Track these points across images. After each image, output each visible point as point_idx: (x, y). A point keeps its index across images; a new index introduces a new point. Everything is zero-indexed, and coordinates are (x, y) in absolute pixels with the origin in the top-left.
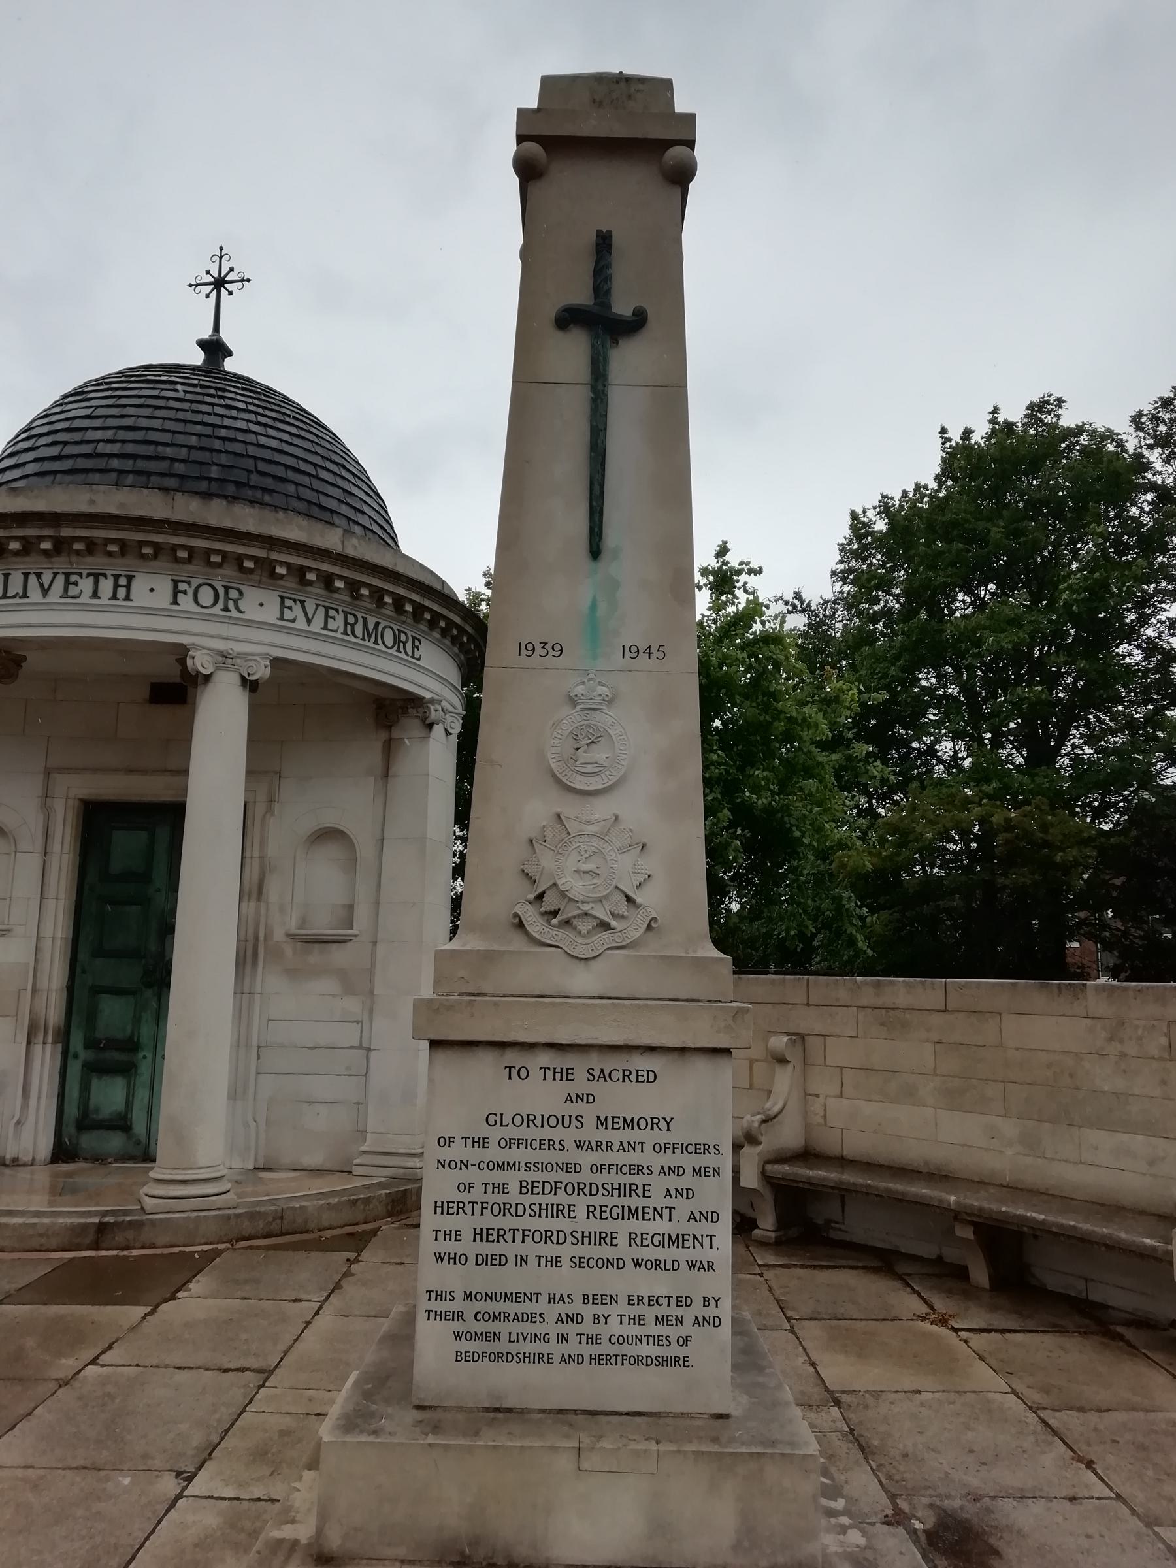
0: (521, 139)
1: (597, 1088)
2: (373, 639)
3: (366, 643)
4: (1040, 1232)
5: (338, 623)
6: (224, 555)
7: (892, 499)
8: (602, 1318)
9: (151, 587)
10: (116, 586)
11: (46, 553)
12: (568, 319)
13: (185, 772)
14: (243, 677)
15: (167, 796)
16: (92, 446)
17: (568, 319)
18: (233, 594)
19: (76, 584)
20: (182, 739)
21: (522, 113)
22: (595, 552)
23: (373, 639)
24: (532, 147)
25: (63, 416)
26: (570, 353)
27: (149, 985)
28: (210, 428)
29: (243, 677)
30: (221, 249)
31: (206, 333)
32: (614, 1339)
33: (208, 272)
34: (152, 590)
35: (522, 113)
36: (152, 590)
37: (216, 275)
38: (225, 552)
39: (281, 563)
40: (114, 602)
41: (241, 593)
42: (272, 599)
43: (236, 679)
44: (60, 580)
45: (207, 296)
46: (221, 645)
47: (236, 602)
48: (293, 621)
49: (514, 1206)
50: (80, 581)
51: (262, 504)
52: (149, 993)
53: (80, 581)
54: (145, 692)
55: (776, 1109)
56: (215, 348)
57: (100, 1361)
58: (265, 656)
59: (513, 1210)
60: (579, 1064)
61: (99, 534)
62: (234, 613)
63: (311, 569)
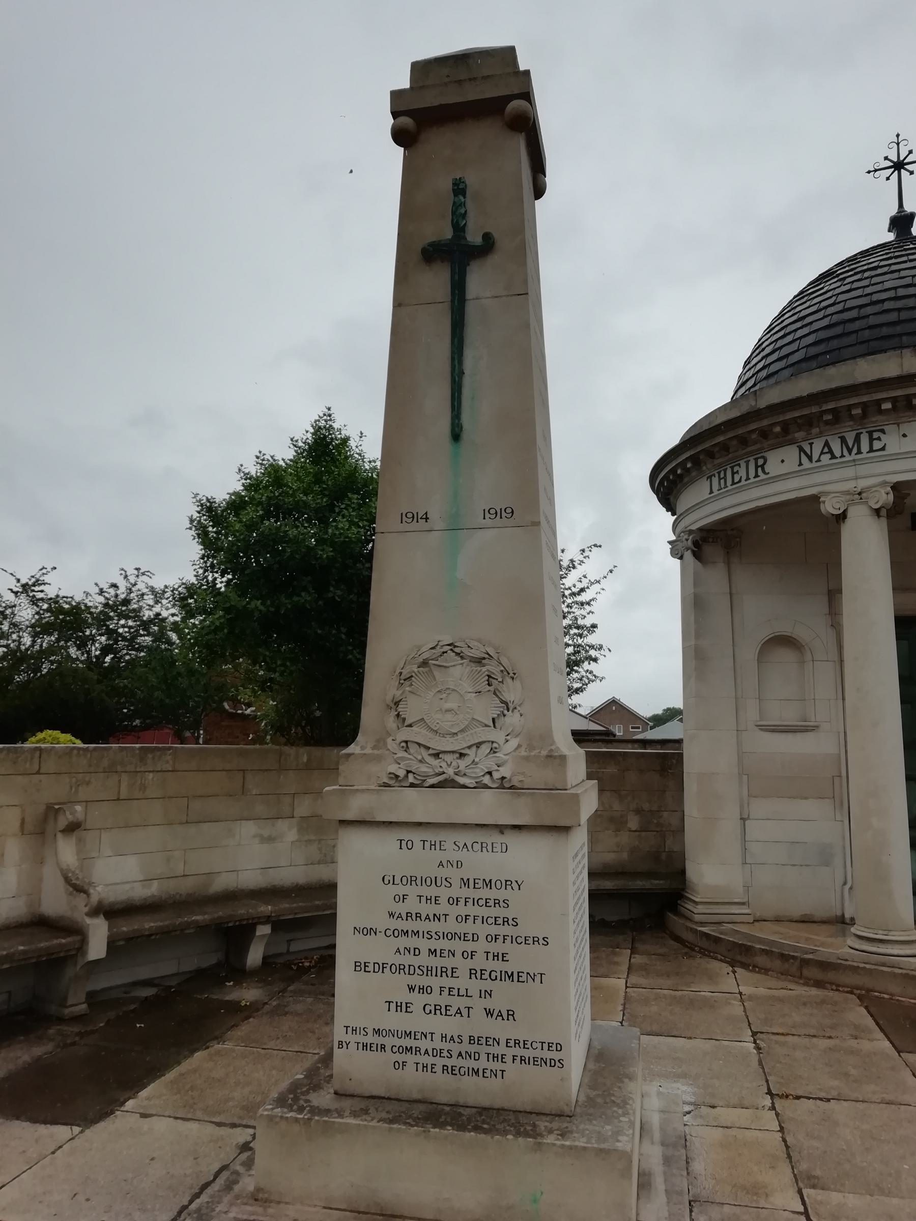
0: (395, 114)
1: (462, 855)
2: (855, 450)
8: (344, 1044)
9: (782, 461)
10: (720, 479)
12: (432, 253)
16: (854, 336)
17: (432, 253)
18: (760, 462)
21: (396, 96)
22: (456, 436)
23: (855, 450)
24: (406, 120)
25: (799, 324)
26: (436, 281)
28: (893, 291)
30: (898, 136)
31: (894, 211)
32: (395, 1049)
33: (886, 158)
34: (783, 461)
35: (396, 96)
36: (783, 461)
37: (895, 160)
38: (864, 403)
39: (885, 400)
41: (763, 457)
42: (790, 454)
45: (888, 179)
46: (849, 486)
47: (762, 467)
48: (883, 449)
49: (407, 967)
56: (901, 222)
59: (407, 970)
60: (449, 838)
62: (762, 476)
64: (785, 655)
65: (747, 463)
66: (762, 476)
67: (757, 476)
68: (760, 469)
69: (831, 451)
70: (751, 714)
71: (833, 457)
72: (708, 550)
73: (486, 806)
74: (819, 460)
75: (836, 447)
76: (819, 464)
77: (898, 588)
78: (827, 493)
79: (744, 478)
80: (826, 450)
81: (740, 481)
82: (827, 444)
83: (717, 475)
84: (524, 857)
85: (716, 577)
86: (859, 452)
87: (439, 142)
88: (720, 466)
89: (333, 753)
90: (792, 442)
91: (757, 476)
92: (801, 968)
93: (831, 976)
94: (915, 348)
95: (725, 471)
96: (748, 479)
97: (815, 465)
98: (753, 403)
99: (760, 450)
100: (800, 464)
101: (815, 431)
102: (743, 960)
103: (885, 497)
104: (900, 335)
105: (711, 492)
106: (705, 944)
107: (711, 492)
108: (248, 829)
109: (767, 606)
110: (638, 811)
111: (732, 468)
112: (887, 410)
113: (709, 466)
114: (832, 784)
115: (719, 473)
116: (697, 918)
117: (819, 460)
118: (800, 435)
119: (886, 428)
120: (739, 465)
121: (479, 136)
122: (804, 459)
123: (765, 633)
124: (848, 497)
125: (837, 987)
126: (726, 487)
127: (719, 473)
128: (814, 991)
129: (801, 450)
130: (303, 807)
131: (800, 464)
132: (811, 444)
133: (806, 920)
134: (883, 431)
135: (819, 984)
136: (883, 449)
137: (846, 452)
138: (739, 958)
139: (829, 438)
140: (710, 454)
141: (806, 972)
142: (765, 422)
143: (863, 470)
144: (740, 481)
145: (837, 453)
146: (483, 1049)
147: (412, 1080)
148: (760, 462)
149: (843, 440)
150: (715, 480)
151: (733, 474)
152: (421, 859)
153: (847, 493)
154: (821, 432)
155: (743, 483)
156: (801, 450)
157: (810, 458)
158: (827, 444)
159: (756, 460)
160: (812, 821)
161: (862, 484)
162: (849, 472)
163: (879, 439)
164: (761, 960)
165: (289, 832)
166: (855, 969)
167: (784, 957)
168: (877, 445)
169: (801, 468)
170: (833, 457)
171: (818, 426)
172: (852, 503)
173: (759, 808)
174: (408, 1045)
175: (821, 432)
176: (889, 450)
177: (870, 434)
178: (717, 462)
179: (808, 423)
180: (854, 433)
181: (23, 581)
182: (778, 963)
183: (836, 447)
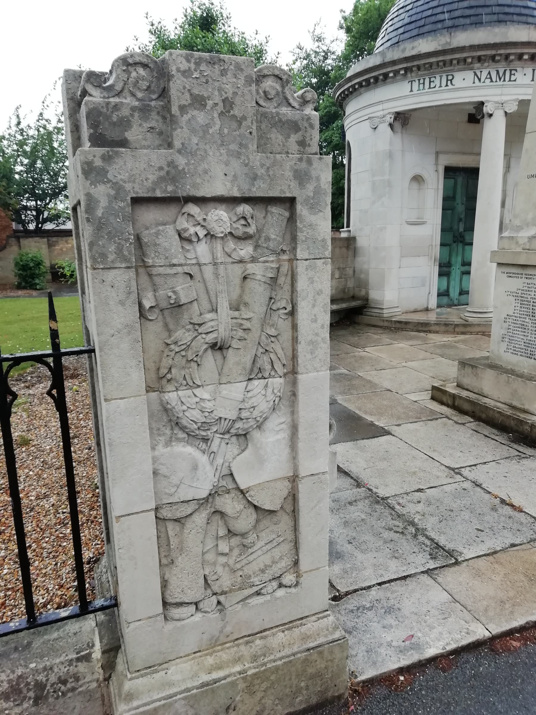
3: (499, 83)
4: (439, 290)
5: (415, 85)
6: (473, 58)
7: (205, 5)
9: (463, 79)
10: (419, 84)
11: (392, 77)
13: (479, 154)
14: (506, 112)
15: (473, 165)
18: (450, 78)
19: (514, 74)
20: (478, 140)
27: (454, 242)
29: (506, 112)
40: (419, 92)
41: (452, 75)
42: (469, 75)
43: (503, 114)
44: (508, 73)
47: (451, 80)
48: (515, 80)
50: (516, 73)
51: (528, 23)
52: (455, 245)
53: (516, 73)
54: (466, 118)
55: (150, 318)
57: (284, 408)
58: (515, 100)
61: (448, 57)
62: (450, 86)
63: (468, 57)
65: (441, 77)
66: (450, 86)
67: (447, 85)
68: (449, 82)
69: (491, 78)
71: (492, 81)
74: (484, 82)
75: (494, 75)
76: (484, 84)
78: (488, 101)
79: (438, 85)
80: (489, 76)
81: (435, 87)
82: (489, 73)
83: (417, 81)
86: (504, 80)
88: (421, 76)
90: (471, 69)
91: (447, 85)
92: (454, 328)
93: (468, 329)
94: (535, 25)
95: (424, 79)
96: (440, 86)
97: (481, 84)
98: (448, 40)
99: (453, 71)
100: (474, 83)
101: (486, 64)
102: (424, 329)
104: (513, 14)
105: (411, 91)
106: (398, 325)
107: (411, 91)
110: (339, 269)
111: (430, 78)
112: (526, 60)
113: (413, 74)
115: (419, 80)
116: (385, 315)
117: (484, 82)
118: (477, 65)
119: (518, 69)
120: (435, 77)
122: (476, 80)
124: (497, 105)
125: (471, 333)
126: (424, 88)
127: (419, 80)
128: (462, 337)
129: (475, 74)
131: (474, 83)
132: (481, 72)
133: (415, 311)
134: (516, 70)
135: (463, 333)
136: (515, 80)
137: (498, 80)
138: (421, 329)
139: (491, 70)
140: (419, 68)
141: (457, 330)
142: (465, 55)
143: (505, 90)
144: (435, 87)
145: (494, 80)
146: (529, 355)
148: (450, 78)
149: (498, 72)
150: (415, 85)
151: (430, 82)
153: (497, 102)
154: (488, 66)
155: (437, 89)
156: (475, 74)
157: (480, 80)
158: (489, 73)
159: (447, 76)
161: (505, 98)
162: (498, 91)
163: (514, 74)
164: (433, 328)
166: (479, 325)
167: (446, 325)
168: (513, 78)
169: (474, 85)
170: (492, 81)
171: (488, 62)
172: (497, 108)
175: (488, 66)
176: (518, 82)
177: (511, 71)
178: (420, 73)
180: (504, 69)
182: (443, 328)
183: (494, 75)
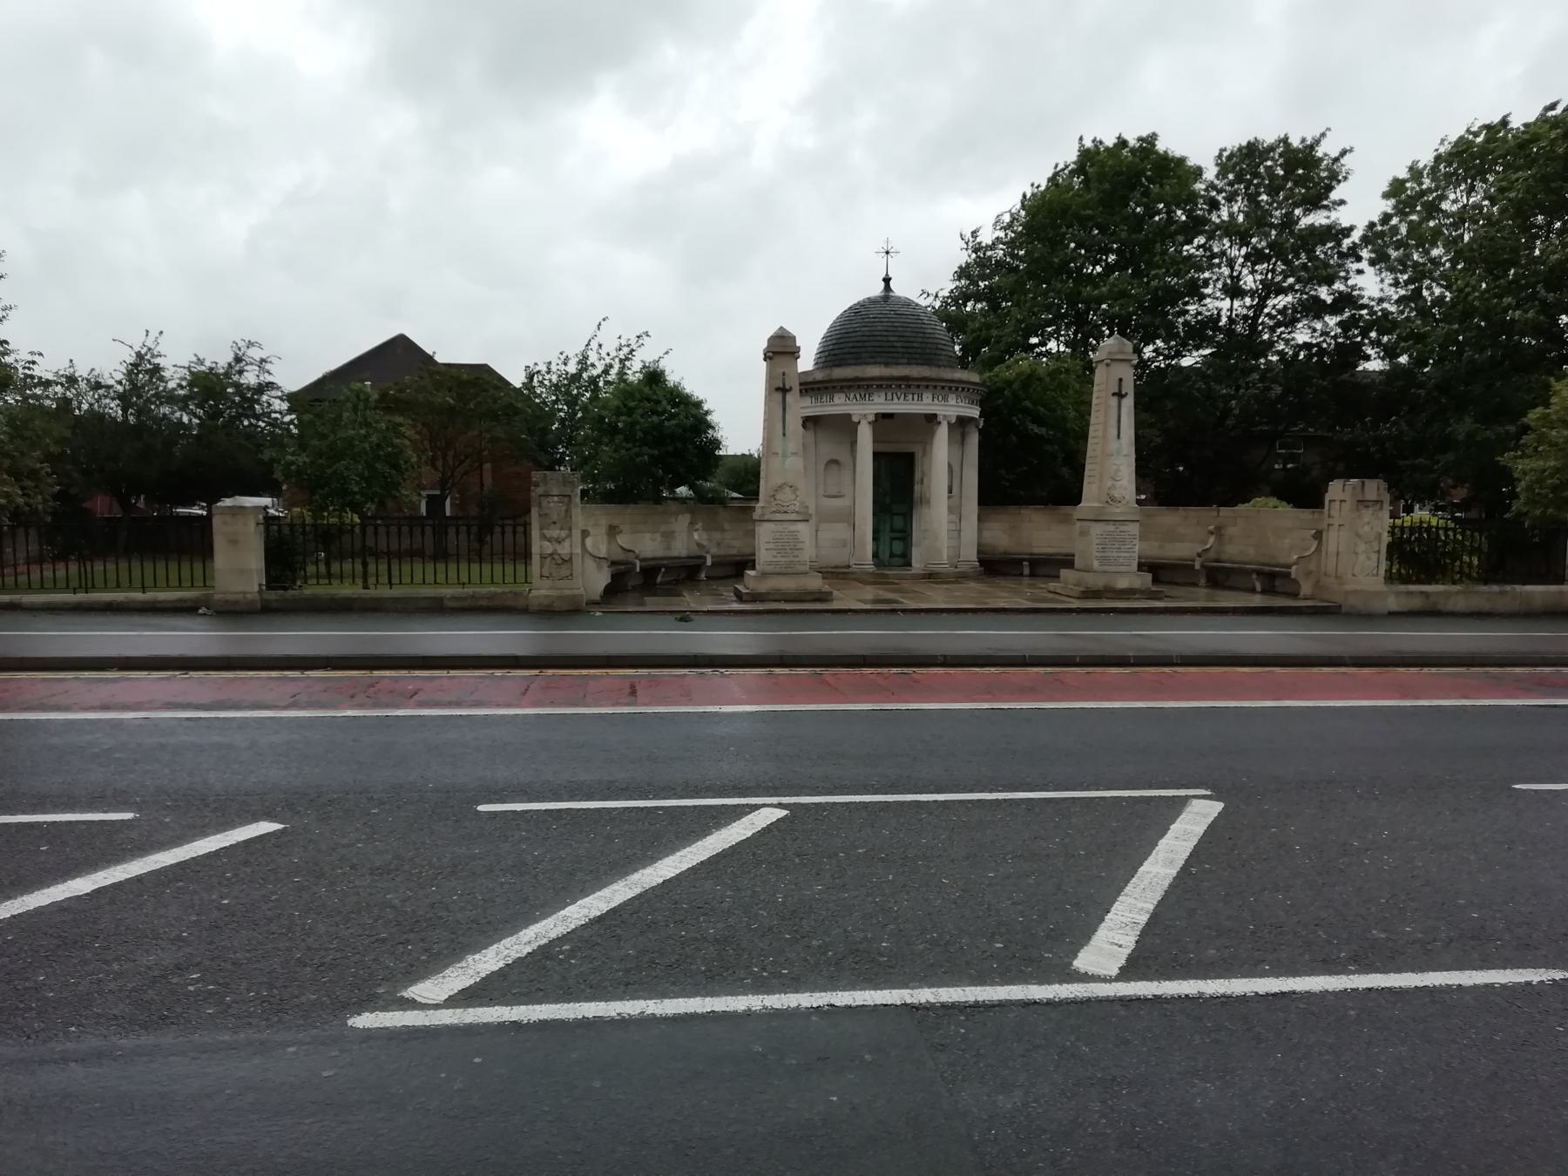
9: (839, 398)
26: (779, 396)
42: (843, 396)
64: (835, 467)
70: (821, 491)
72: (809, 424)
73: (794, 516)
77: (875, 441)
84: (801, 527)
85: (810, 435)
87: (778, 359)
89: (1067, 509)
103: (872, 418)
108: (648, 536)
109: (828, 449)
114: (849, 518)
121: (786, 359)
123: (828, 458)
130: (663, 528)
147: (778, 570)
152: (779, 527)
160: (840, 531)
165: (658, 537)
173: (823, 526)
174: (777, 564)
179: (850, 387)
181: (137, 349)
